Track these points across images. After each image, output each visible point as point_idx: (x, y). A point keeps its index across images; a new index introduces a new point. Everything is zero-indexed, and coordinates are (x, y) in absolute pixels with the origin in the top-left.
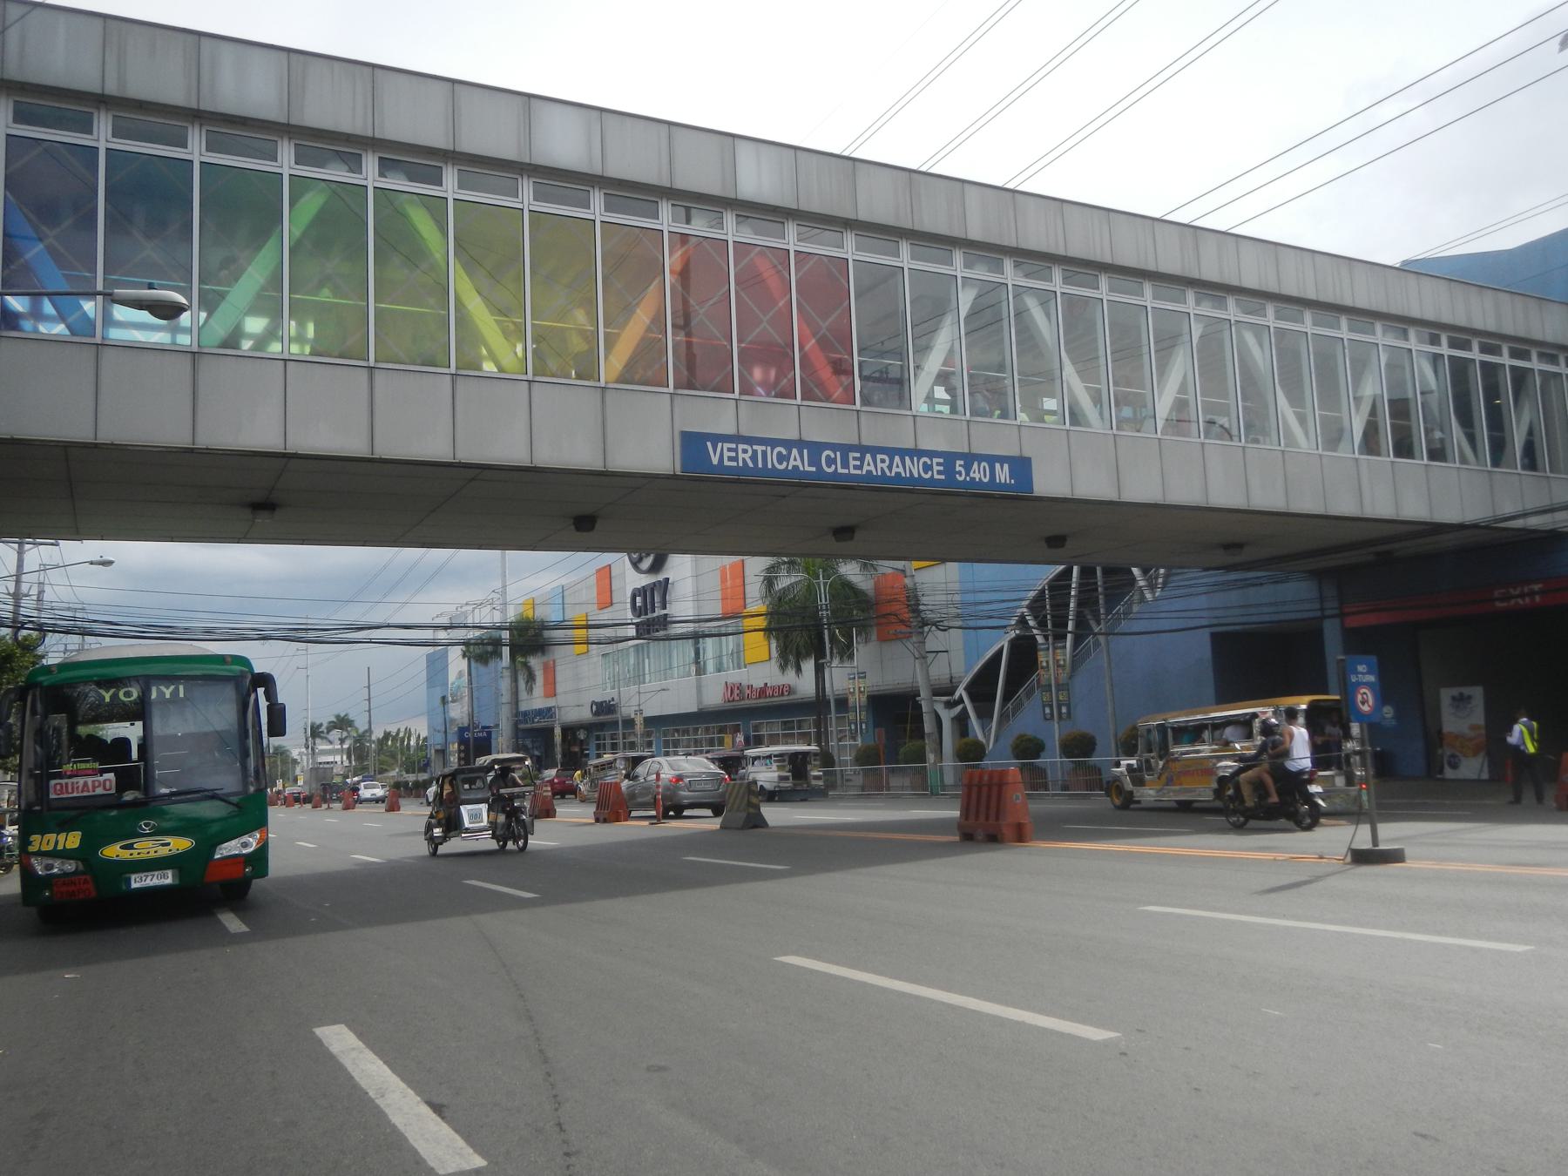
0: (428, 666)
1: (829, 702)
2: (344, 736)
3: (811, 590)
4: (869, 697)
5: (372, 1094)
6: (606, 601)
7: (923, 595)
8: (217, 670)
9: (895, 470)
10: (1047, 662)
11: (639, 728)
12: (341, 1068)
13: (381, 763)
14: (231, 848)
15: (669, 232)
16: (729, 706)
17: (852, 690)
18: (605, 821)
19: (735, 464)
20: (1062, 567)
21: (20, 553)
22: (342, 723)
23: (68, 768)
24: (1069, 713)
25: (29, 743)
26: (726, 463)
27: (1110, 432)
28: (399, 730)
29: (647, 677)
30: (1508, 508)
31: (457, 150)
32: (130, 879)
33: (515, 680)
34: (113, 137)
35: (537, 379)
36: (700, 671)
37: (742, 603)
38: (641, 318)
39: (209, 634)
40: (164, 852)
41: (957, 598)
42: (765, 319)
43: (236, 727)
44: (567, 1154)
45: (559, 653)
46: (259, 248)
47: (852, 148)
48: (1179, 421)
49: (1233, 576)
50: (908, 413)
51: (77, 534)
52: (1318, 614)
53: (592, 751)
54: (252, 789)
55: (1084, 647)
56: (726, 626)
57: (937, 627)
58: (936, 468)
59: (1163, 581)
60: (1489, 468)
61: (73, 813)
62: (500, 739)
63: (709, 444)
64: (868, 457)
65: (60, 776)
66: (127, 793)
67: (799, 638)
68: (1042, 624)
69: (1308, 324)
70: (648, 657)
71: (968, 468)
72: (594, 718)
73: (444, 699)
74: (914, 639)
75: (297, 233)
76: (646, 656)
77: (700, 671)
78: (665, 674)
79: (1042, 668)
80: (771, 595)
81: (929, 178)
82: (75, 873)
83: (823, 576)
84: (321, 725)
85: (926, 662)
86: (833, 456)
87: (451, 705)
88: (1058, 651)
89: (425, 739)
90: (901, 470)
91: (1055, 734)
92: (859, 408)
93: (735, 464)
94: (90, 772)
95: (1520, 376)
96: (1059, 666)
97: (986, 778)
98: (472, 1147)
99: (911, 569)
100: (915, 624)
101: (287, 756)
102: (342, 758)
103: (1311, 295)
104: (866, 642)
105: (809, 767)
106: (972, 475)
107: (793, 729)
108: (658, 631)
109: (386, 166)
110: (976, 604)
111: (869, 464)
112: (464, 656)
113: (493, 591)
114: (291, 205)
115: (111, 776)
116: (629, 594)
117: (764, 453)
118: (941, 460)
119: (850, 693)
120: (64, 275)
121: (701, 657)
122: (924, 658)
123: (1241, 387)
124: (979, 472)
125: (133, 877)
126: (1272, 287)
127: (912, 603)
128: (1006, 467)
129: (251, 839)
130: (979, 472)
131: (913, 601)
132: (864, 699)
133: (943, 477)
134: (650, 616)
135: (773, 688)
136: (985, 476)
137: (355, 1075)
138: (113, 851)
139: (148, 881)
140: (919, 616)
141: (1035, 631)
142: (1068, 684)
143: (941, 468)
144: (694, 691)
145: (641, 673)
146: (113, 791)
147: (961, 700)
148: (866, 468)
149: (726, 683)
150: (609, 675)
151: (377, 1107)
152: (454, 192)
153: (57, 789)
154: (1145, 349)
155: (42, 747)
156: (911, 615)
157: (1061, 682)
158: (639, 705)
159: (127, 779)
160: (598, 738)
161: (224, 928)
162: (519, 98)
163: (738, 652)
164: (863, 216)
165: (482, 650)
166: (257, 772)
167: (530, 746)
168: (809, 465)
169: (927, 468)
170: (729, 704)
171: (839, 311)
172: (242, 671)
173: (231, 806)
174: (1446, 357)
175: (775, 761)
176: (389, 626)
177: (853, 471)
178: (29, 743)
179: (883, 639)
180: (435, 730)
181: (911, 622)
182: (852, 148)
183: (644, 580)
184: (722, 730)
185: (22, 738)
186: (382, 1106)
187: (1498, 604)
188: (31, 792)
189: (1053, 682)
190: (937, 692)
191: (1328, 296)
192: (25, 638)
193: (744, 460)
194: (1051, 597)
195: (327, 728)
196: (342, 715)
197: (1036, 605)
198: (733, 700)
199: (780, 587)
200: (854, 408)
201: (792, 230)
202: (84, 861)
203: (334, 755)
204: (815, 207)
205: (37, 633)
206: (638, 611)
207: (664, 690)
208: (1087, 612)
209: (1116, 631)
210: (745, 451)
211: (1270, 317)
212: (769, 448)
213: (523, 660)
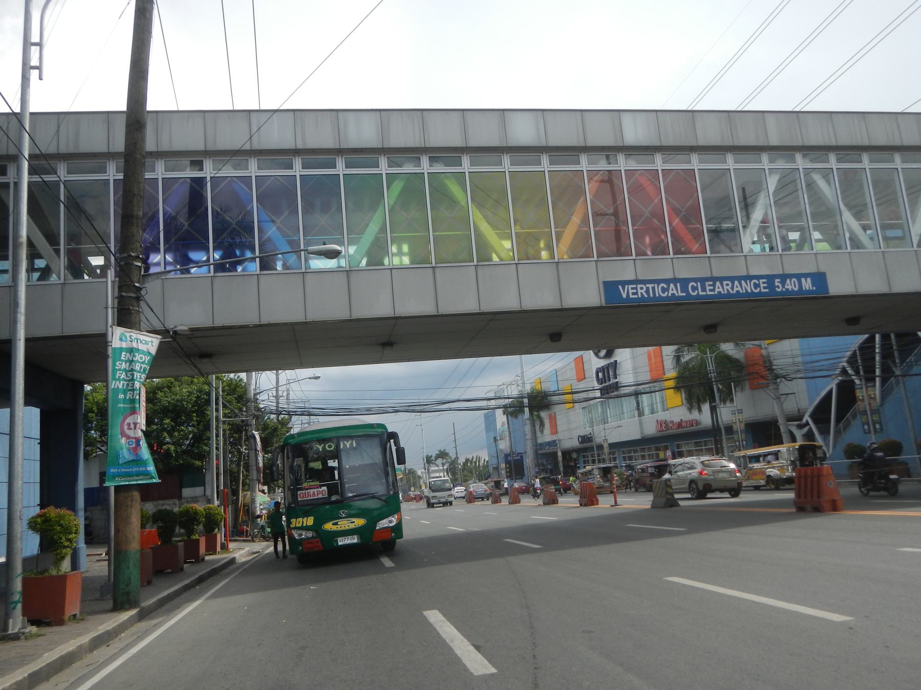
0: (485, 421)
1: (720, 429)
3: (703, 363)
5: (447, 641)
6: (582, 377)
7: (774, 360)
8: (370, 431)
9: (735, 289)
10: (874, 394)
11: (606, 450)
12: (435, 629)
13: (465, 476)
14: (384, 523)
15: (587, 170)
16: (660, 434)
18: (586, 505)
19: (636, 296)
20: (867, 336)
21: (277, 375)
22: (443, 455)
23: (305, 485)
24: (881, 429)
25: (287, 473)
26: (631, 296)
27: (879, 250)
28: (473, 457)
29: (609, 419)
32: (337, 540)
33: (533, 425)
34: (302, 169)
36: (641, 414)
37: (662, 371)
38: (576, 220)
39: (369, 411)
40: (352, 526)
41: (799, 359)
43: (382, 460)
44: (535, 668)
45: (557, 409)
46: (375, 211)
47: (693, 104)
50: (742, 254)
51: (302, 366)
53: (581, 464)
54: (392, 492)
56: (650, 387)
58: (762, 285)
61: (310, 507)
62: (527, 460)
63: (620, 287)
64: (718, 284)
65: (301, 489)
66: (333, 496)
68: (857, 372)
71: (783, 283)
72: (582, 445)
74: (771, 387)
75: (392, 203)
76: (607, 407)
77: (641, 414)
79: (860, 400)
82: (312, 537)
83: (710, 352)
84: (432, 456)
85: (780, 401)
86: (695, 285)
87: (500, 442)
88: (870, 389)
89: (487, 462)
90: (739, 289)
93: (636, 296)
94: (315, 487)
98: (491, 664)
99: (765, 344)
100: (771, 378)
101: (416, 474)
102: (444, 474)
106: (786, 287)
107: (702, 446)
108: (613, 392)
109: (432, 160)
110: (812, 362)
111: (719, 288)
112: (504, 413)
113: (517, 376)
114: (388, 188)
115: (325, 488)
116: (594, 371)
117: (653, 288)
118: (765, 280)
119: (734, 423)
120: (285, 240)
122: (779, 398)
124: (791, 285)
125: (339, 539)
127: (768, 364)
128: (809, 280)
129: (393, 519)
130: (791, 285)
131: (768, 363)
132: (743, 426)
133: (767, 290)
134: (607, 384)
135: (686, 422)
136: (795, 287)
137: (441, 633)
138: (329, 526)
139: (346, 541)
141: (854, 377)
142: (878, 410)
143: (766, 285)
145: (606, 417)
146: (326, 496)
147: (807, 424)
148: (717, 290)
149: (657, 420)
150: (587, 419)
151: (450, 646)
153: (302, 496)
154: (899, 194)
155: (293, 475)
156: (767, 372)
157: (873, 408)
158: (605, 437)
159: (332, 490)
160: (584, 457)
161: (383, 565)
164: (701, 142)
165: (514, 409)
166: (393, 484)
167: (545, 463)
168: (681, 293)
169: (756, 286)
170: (660, 433)
171: (693, 199)
172: (382, 432)
173: (382, 502)
176: (459, 401)
177: (709, 293)
178: (287, 473)
179: (753, 388)
180: (492, 456)
182: (693, 104)
183: (603, 363)
184: (658, 449)
185: (284, 471)
186: (452, 646)
188: (290, 496)
189: (739, 429)
190: (790, 419)
192: (282, 419)
193: (641, 293)
194: (861, 354)
195: (435, 457)
197: (852, 361)
198: (663, 431)
199: (685, 360)
200: (706, 255)
201: (658, 158)
202: (316, 531)
203: (439, 474)
204: (671, 142)
205: (287, 416)
207: (619, 427)
208: (890, 362)
210: (642, 288)
212: (656, 285)
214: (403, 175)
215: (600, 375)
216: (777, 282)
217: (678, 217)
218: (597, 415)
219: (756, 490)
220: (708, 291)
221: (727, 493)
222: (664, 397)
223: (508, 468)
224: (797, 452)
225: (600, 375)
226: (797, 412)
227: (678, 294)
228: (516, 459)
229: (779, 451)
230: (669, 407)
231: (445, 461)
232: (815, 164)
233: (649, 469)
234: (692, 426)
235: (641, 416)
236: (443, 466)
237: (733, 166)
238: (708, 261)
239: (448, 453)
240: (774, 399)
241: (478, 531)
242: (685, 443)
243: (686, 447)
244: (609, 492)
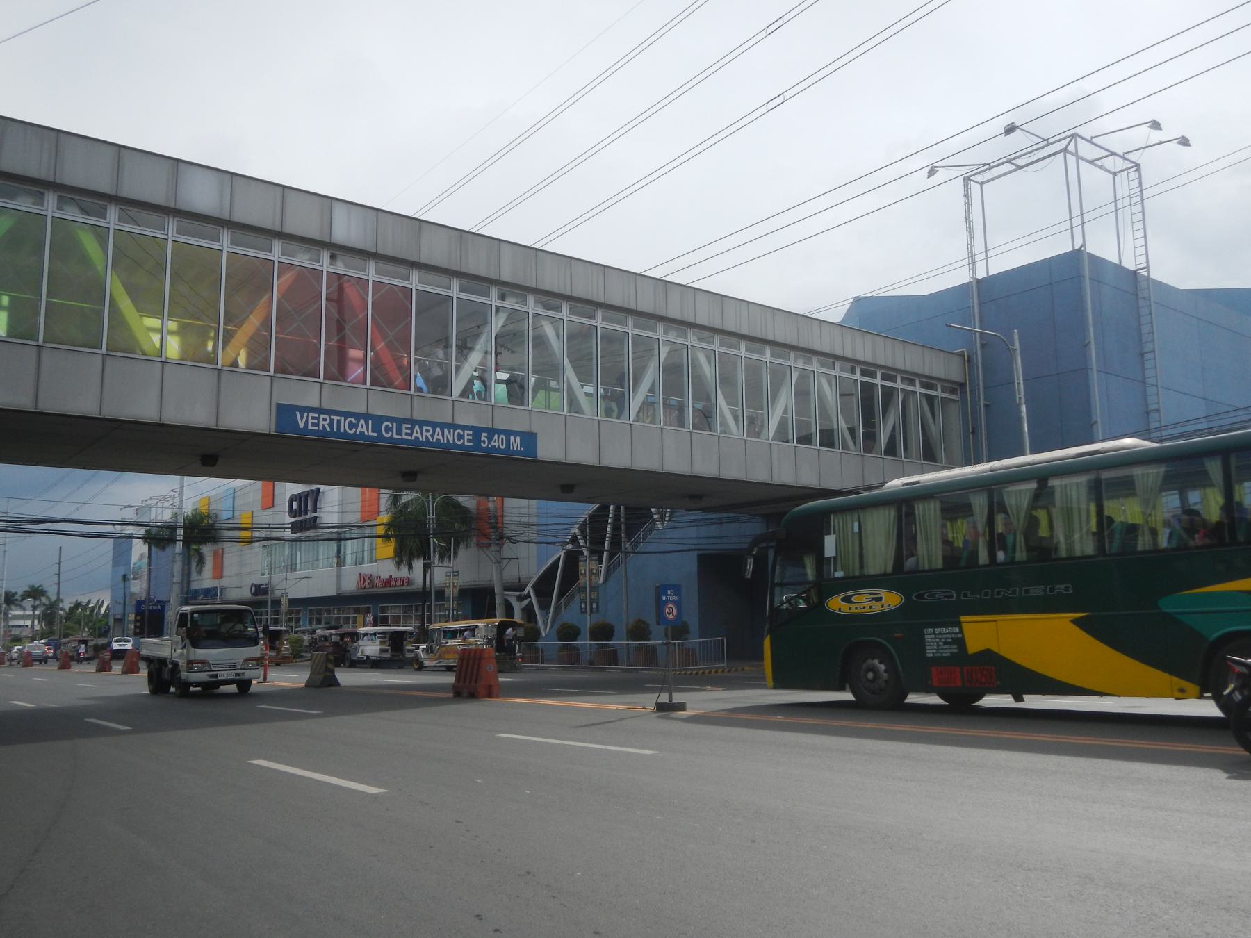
2: (36, 604)
3: (423, 506)
4: (460, 590)
9: (436, 437)
10: (449, 583)
11: (284, 607)
13: (68, 628)
16: (361, 592)
17: (448, 584)
19: (316, 428)
22: (35, 593)
26: (310, 427)
28: (90, 601)
36: (341, 563)
38: (253, 322)
41: (534, 520)
47: (420, 213)
50: (450, 398)
55: (616, 560)
58: (466, 437)
63: (298, 413)
64: (417, 428)
69: (742, 351)
70: (300, 550)
71: (490, 438)
73: (125, 578)
74: (493, 548)
77: (341, 563)
78: (313, 564)
79: (582, 574)
81: (476, 236)
84: (16, 593)
86: (391, 426)
88: (593, 563)
91: (587, 622)
93: (316, 428)
95: (888, 394)
97: (472, 654)
102: (33, 623)
103: (745, 331)
104: (467, 547)
105: (405, 643)
106: (493, 443)
110: (546, 525)
113: (172, 490)
116: (287, 499)
117: (339, 422)
118: (471, 432)
121: (342, 552)
123: (745, 377)
126: (717, 324)
127: (493, 521)
128: (518, 439)
132: (456, 591)
133: (471, 444)
134: (303, 518)
136: (502, 445)
143: (471, 438)
144: (334, 579)
147: (528, 596)
148: (415, 435)
149: (360, 574)
152: (115, 224)
156: (491, 530)
157: (593, 585)
164: (424, 260)
165: (159, 537)
168: (372, 432)
175: (379, 638)
177: (405, 437)
180: (116, 602)
181: (491, 536)
182: (420, 213)
190: (507, 588)
196: (36, 585)
199: (403, 501)
204: (389, 252)
206: (294, 513)
209: (636, 551)
210: (324, 420)
211: (716, 345)
212: (343, 418)
214: (13, 211)
215: (295, 505)
216: (484, 436)
217: (384, 341)
218: (282, 559)
219: (449, 671)
220: (404, 434)
223: (139, 621)
224: (495, 630)
225: (295, 505)
226: (518, 580)
227: (368, 432)
228: (154, 610)
229: (477, 627)
230: (378, 558)
231: (37, 603)
233: (333, 637)
235: (340, 566)
236: (33, 611)
237: (327, 267)
238: (410, 399)
239: (45, 591)
240: (494, 563)
241: (56, 708)
243: (393, 611)
244: (274, 664)
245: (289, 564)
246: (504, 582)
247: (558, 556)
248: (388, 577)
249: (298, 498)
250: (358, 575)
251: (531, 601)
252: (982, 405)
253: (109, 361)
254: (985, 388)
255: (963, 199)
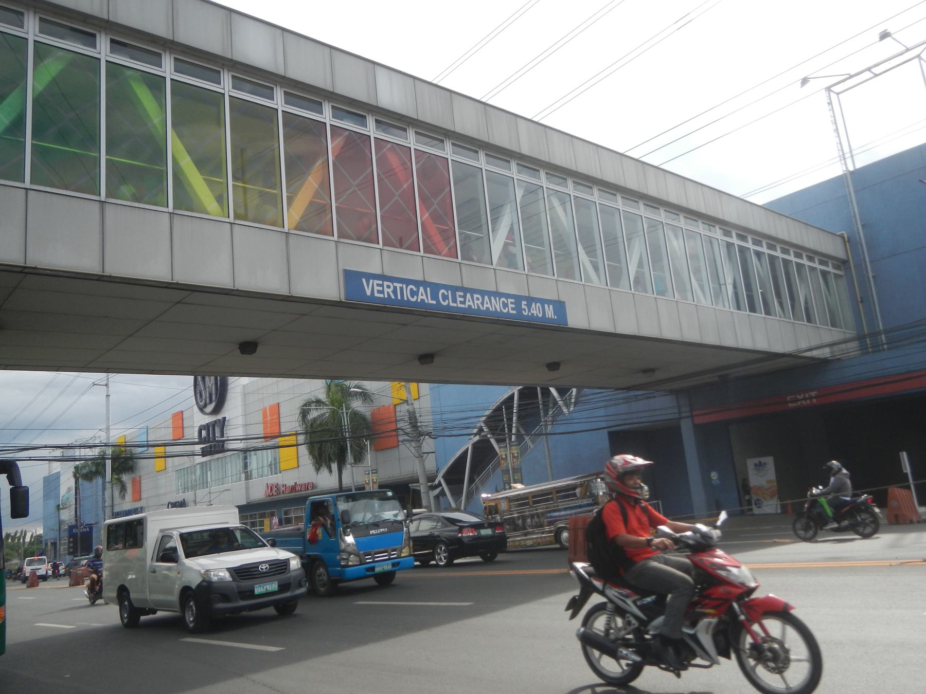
9: (485, 306)
10: (506, 455)
16: (269, 499)
18: (73, 585)
26: (376, 295)
30: (804, 346)
31: (175, 40)
35: (237, 222)
36: (248, 477)
42: (397, 194)
48: (639, 281)
49: (632, 393)
52: (677, 416)
57: (429, 436)
58: (510, 306)
59: (575, 401)
60: (792, 321)
63: (364, 280)
64: (468, 296)
67: (331, 449)
71: (529, 306)
75: (40, 88)
77: (248, 477)
80: (305, 424)
88: (513, 448)
92: (460, 262)
93: (382, 296)
96: (514, 457)
106: (532, 312)
116: (197, 429)
117: (401, 289)
118: (513, 301)
119: (366, 483)
124: (536, 310)
128: (551, 307)
130: (536, 310)
133: (515, 312)
135: (301, 485)
136: (540, 313)
140: (417, 430)
143: (513, 306)
144: (244, 491)
145: (205, 481)
147: (440, 484)
148: (467, 303)
149: (267, 484)
150: (181, 483)
158: (210, 501)
162: (223, 11)
163: (275, 464)
169: (505, 305)
174: (766, 254)
183: (207, 420)
184: (263, 516)
187: (790, 405)
191: (711, 213)
193: (388, 293)
199: (311, 417)
210: (388, 287)
212: (404, 286)
213: (117, 477)
214: (61, 53)
220: (458, 302)
221: (479, 557)
222: (278, 459)
223: (72, 542)
225: (204, 433)
232: (551, 185)
234: (308, 489)
240: (417, 457)
242: (294, 509)
245: (201, 482)
246: (427, 473)
247: (467, 447)
248: (293, 484)
249: (206, 428)
250: (265, 485)
251: (443, 489)
252: (871, 276)
253: (176, 220)
254: (871, 262)
255: (827, 107)
